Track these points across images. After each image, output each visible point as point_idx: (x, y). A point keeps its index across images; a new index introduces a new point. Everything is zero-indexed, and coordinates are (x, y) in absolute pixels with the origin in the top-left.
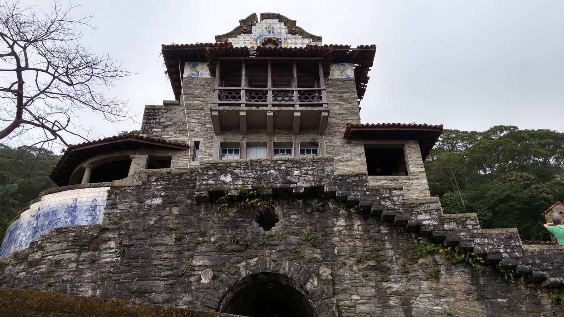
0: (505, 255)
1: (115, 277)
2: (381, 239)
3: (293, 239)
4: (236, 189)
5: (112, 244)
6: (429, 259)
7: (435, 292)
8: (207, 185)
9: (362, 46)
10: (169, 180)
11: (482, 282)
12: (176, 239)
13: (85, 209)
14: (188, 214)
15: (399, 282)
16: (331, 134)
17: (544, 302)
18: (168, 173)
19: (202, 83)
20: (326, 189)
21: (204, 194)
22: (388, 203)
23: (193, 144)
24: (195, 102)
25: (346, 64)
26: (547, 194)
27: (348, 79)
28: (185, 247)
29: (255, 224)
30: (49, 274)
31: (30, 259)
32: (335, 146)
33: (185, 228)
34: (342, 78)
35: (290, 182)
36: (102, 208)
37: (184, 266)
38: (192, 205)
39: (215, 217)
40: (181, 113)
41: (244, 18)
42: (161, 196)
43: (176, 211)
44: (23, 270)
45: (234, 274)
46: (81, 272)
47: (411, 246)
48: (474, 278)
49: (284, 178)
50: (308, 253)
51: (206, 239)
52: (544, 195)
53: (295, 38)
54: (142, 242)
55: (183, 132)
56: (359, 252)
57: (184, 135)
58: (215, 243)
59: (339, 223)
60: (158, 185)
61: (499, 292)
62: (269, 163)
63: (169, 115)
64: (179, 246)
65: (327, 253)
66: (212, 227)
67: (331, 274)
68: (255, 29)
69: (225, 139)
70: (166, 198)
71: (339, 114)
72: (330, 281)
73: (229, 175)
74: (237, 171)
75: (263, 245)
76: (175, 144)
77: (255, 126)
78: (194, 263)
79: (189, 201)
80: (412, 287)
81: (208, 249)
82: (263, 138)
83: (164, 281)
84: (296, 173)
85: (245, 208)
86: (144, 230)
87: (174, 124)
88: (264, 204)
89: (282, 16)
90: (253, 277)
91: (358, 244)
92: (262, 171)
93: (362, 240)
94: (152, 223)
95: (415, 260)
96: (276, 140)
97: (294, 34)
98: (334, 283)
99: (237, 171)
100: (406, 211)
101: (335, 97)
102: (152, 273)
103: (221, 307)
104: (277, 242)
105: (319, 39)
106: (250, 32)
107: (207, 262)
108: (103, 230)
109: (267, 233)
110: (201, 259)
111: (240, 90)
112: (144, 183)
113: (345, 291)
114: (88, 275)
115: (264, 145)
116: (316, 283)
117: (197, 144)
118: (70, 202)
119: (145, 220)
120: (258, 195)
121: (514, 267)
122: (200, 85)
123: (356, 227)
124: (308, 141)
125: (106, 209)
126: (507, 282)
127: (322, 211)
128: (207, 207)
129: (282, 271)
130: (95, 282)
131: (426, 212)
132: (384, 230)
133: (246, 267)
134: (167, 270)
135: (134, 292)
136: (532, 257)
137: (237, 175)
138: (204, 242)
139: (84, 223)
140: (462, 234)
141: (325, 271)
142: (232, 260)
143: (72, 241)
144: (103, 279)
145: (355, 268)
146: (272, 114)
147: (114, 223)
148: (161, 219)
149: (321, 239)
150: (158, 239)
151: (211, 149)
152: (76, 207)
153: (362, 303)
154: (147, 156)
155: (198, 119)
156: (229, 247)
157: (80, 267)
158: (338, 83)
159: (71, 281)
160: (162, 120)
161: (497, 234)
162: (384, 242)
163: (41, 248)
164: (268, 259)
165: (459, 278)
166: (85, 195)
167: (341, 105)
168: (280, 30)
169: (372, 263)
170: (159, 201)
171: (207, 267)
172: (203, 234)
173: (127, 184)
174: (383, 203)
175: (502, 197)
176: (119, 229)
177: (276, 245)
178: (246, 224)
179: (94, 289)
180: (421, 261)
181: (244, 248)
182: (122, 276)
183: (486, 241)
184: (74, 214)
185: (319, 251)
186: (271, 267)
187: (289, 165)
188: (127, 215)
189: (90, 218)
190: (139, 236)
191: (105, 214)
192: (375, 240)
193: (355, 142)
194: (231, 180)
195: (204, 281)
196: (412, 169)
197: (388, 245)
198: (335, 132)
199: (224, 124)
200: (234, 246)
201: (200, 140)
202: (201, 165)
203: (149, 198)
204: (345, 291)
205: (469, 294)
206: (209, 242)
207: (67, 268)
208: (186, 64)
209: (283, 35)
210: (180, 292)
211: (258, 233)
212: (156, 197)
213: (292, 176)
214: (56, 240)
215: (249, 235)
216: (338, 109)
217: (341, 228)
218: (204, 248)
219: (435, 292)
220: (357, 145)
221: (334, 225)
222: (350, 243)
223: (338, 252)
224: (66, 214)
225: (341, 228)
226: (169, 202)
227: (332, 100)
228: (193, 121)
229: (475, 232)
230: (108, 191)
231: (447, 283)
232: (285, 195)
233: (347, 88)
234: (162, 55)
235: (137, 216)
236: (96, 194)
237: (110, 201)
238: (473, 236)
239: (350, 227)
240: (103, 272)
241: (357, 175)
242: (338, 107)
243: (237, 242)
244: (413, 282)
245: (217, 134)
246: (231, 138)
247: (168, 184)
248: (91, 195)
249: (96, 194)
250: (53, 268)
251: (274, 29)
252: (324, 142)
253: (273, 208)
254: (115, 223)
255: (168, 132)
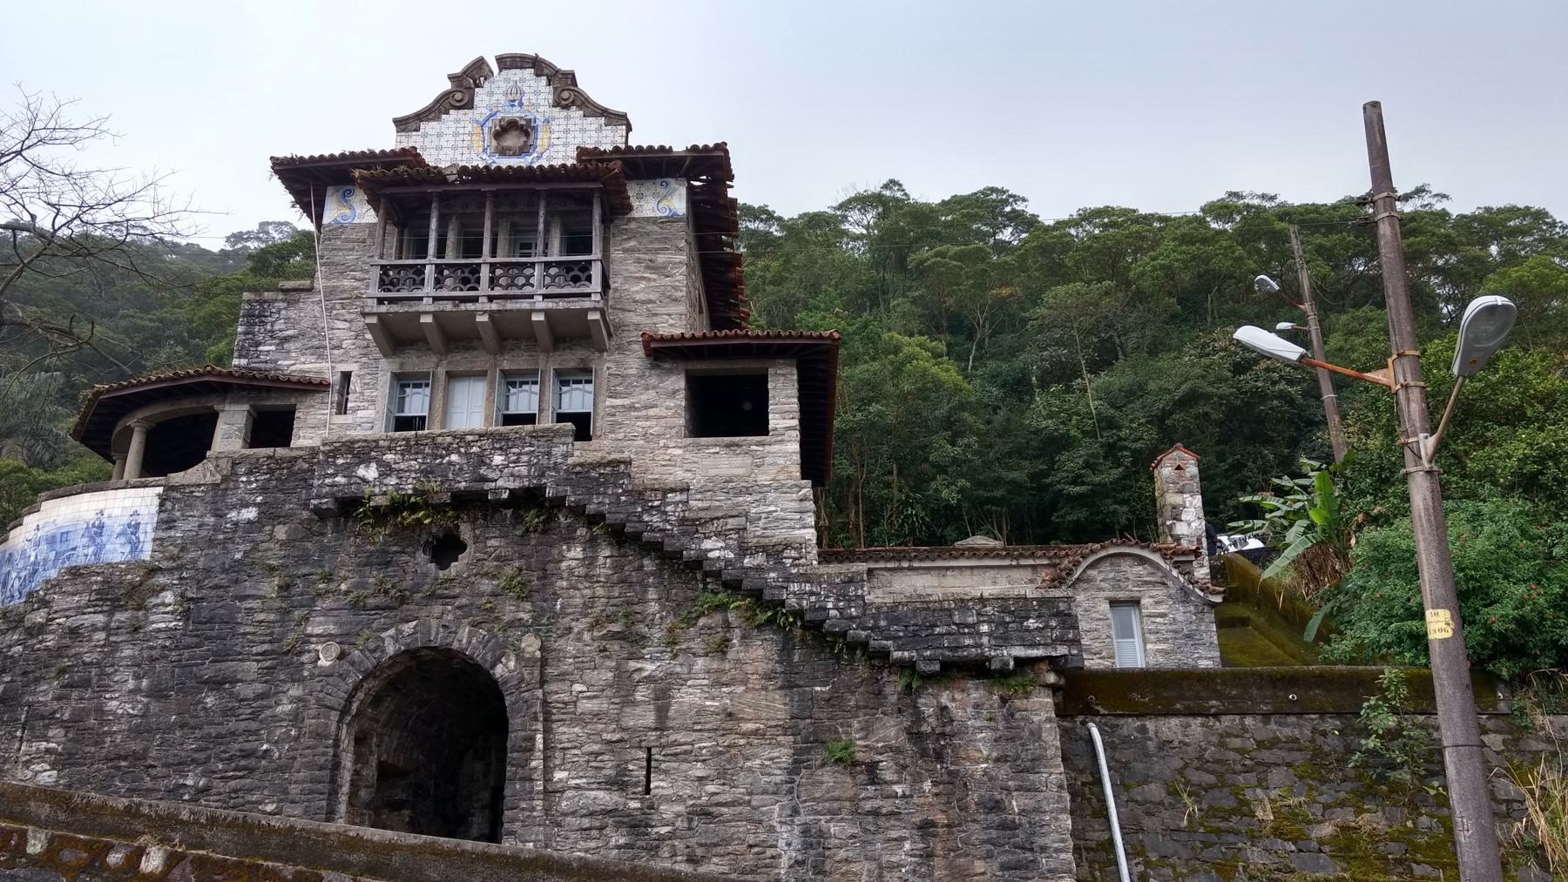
0: (833, 613)
1: (173, 655)
2: (641, 583)
3: (486, 585)
4: (385, 493)
5: (168, 597)
6: (718, 618)
7: (714, 676)
8: (332, 486)
9: (695, 148)
10: (271, 471)
11: (796, 658)
12: (280, 587)
13: (118, 530)
14: (302, 540)
15: (658, 659)
16: (621, 349)
17: (888, 690)
18: (269, 457)
19: (361, 235)
20: (549, 493)
21: (327, 503)
22: (655, 519)
23: (338, 377)
24: (346, 283)
25: (672, 181)
26: (1291, 382)
27: (672, 219)
28: (295, 598)
29: (421, 557)
30: (59, 652)
31: (27, 624)
32: (628, 376)
33: (297, 565)
34: (659, 214)
35: (485, 479)
36: (149, 528)
37: (292, 636)
38: (310, 520)
39: (351, 544)
40: (317, 308)
41: (458, 69)
42: (255, 505)
43: (281, 532)
44: (18, 643)
45: (374, 651)
46: (115, 647)
47: (690, 594)
48: (785, 651)
49: (474, 471)
50: (510, 610)
51: (332, 586)
52: (1282, 386)
53: (567, 118)
54: (221, 592)
55: (318, 352)
56: (599, 605)
57: (321, 357)
58: (347, 593)
59: (572, 554)
60: (250, 483)
61: (820, 674)
62: (449, 439)
63: (292, 313)
64: (284, 598)
65: (543, 609)
66: (343, 564)
67: (542, 649)
68: (481, 97)
69: (402, 365)
70: (264, 508)
71: (644, 302)
72: (536, 660)
73: (374, 465)
74: (389, 457)
75: (433, 596)
76: (299, 382)
77: (455, 337)
78: (309, 630)
79: (305, 514)
80: (678, 669)
81: (335, 605)
82: (480, 361)
83: (258, 661)
84: (498, 459)
85: (405, 528)
86: (225, 571)
87: (303, 334)
88: (441, 519)
89: (543, 61)
90: (411, 654)
91: (600, 591)
92: (435, 457)
93: (609, 584)
94: (238, 556)
95: (691, 621)
96: (506, 366)
97: (566, 107)
98: (544, 663)
99: (389, 457)
100: (683, 534)
101: (639, 261)
102: (237, 649)
103: (355, 706)
104: (457, 591)
105: (618, 119)
106: (469, 105)
107: (332, 629)
108: (153, 571)
109: (441, 574)
110: (321, 624)
111: (424, 266)
112: (225, 479)
113: (562, 677)
114: (127, 652)
115: (481, 375)
116: (512, 664)
117: (346, 376)
118: (91, 516)
119: (227, 552)
120: (427, 505)
121: (844, 634)
122: (357, 241)
123: (601, 560)
124: (571, 365)
125: (156, 529)
126: (838, 658)
127: (544, 532)
128: (337, 525)
129: (455, 646)
130: (139, 666)
131: (718, 534)
132: (649, 564)
133: (395, 639)
134: (263, 642)
135: (206, 682)
136: (875, 618)
137: (388, 465)
138: (327, 592)
139: (117, 558)
140: (772, 575)
141: (531, 645)
142: (374, 625)
143: (97, 592)
144: (152, 660)
145: (587, 636)
146: (485, 318)
147: (172, 560)
148: (255, 549)
149: (535, 585)
150: (248, 587)
151: (374, 387)
152: (101, 526)
153: (589, 698)
154: (246, 407)
155: (350, 321)
156: (371, 601)
157: (113, 639)
158: (650, 228)
159: (98, 663)
160: (277, 327)
161: (829, 575)
162: (645, 587)
163: (45, 603)
164: (434, 623)
165: (760, 652)
166: (118, 503)
167: (649, 280)
168: (538, 93)
169: (615, 628)
170: (250, 514)
171: (330, 636)
172: (328, 578)
173: (194, 480)
174: (646, 518)
175: (1178, 395)
176: (180, 568)
177: (455, 597)
178: (405, 558)
179: (138, 677)
180: (701, 622)
181: (398, 603)
182: (186, 654)
183: (808, 587)
184: (98, 540)
185: (528, 606)
186: (437, 638)
187: (486, 443)
188: (194, 543)
189: (128, 549)
190: (216, 581)
191: (154, 540)
192: (631, 584)
193: (667, 365)
194: (376, 475)
195: (323, 662)
196: (774, 421)
197: (652, 594)
198: (629, 343)
199: (395, 336)
200: (380, 600)
201: (353, 367)
202: (325, 444)
203: (234, 507)
204: (562, 677)
205: (770, 679)
206: (337, 592)
207: (90, 640)
208: (330, 190)
209: (541, 109)
210: (283, 681)
211: (425, 575)
212: (247, 506)
213: (489, 466)
214: (70, 589)
215: (408, 578)
216: (642, 290)
217: (574, 563)
218: (328, 603)
219: (714, 676)
220: (670, 372)
221: (562, 558)
222: (587, 592)
223: (562, 607)
224: (85, 540)
225: (574, 563)
226: (269, 515)
227: (632, 269)
228: (340, 325)
229: (794, 571)
230: (159, 496)
231: (738, 661)
232: (473, 503)
233: (666, 240)
234: (276, 177)
235: (211, 542)
236: (138, 502)
237: (163, 516)
238: (789, 579)
239: (590, 561)
240: (152, 648)
241: (609, 463)
242: (642, 285)
243: (386, 592)
244: (680, 659)
245: (385, 356)
246: (415, 362)
247: (269, 480)
248: (128, 503)
249: (138, 502)
250: (67, 641)
251: (522, 94)
252: (607, 366)
253: (457, 526)
254: (172, 558)
255: (289, 352)
